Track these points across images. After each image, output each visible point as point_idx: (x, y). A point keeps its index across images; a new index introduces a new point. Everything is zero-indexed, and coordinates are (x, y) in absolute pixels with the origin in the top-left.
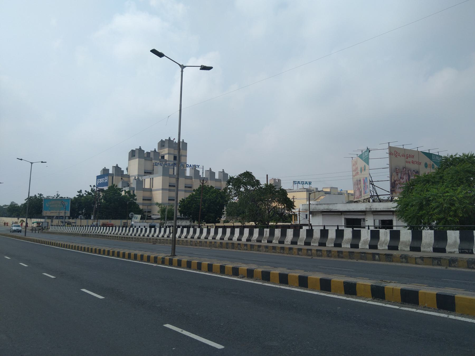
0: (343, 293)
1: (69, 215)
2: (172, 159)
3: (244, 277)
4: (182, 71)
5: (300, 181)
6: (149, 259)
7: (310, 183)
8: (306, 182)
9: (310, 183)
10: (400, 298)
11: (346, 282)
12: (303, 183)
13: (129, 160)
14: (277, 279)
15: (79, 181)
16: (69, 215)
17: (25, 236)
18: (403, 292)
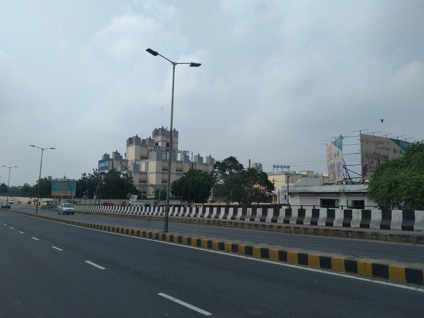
0: (319, 266)
2: (165, 145)
3: (230, 251)
4: (174, 68)
5: (280, 165)
7: (288, 167)
8: (285, 166)
9: (288, 167)
12: (282, 167)
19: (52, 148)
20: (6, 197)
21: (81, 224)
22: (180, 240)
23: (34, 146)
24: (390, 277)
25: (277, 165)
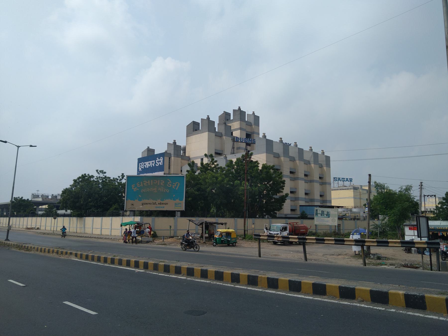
0: (288, 290)
1: (183, 209)
2: (244, 137)
3: (228, 282)
4: (18, 149)
5: (341, 177)
6: (99, 259)
7: (351, 180)
8: (347, 179)
9: (351, 180)
10: (370, 298)
11: (345, 288)
12: (343, 180)
13: (187, 136)
14: (368, 296)
15: (56, 183)
16: (183, 209)
17: (306, 259)
18: (407, 297)
19: (31, 146)
20: (240, 221)
21: (43, 250)
22: (146, 266)
23: (6, 142)
24: (327, 294)
25: (338, 177)
